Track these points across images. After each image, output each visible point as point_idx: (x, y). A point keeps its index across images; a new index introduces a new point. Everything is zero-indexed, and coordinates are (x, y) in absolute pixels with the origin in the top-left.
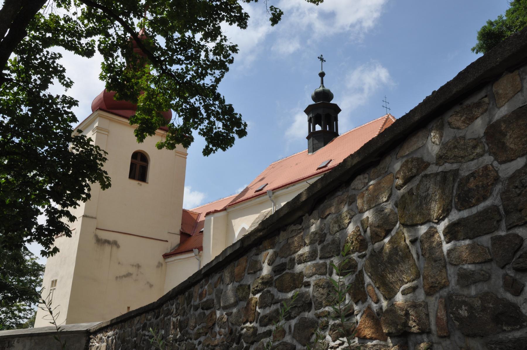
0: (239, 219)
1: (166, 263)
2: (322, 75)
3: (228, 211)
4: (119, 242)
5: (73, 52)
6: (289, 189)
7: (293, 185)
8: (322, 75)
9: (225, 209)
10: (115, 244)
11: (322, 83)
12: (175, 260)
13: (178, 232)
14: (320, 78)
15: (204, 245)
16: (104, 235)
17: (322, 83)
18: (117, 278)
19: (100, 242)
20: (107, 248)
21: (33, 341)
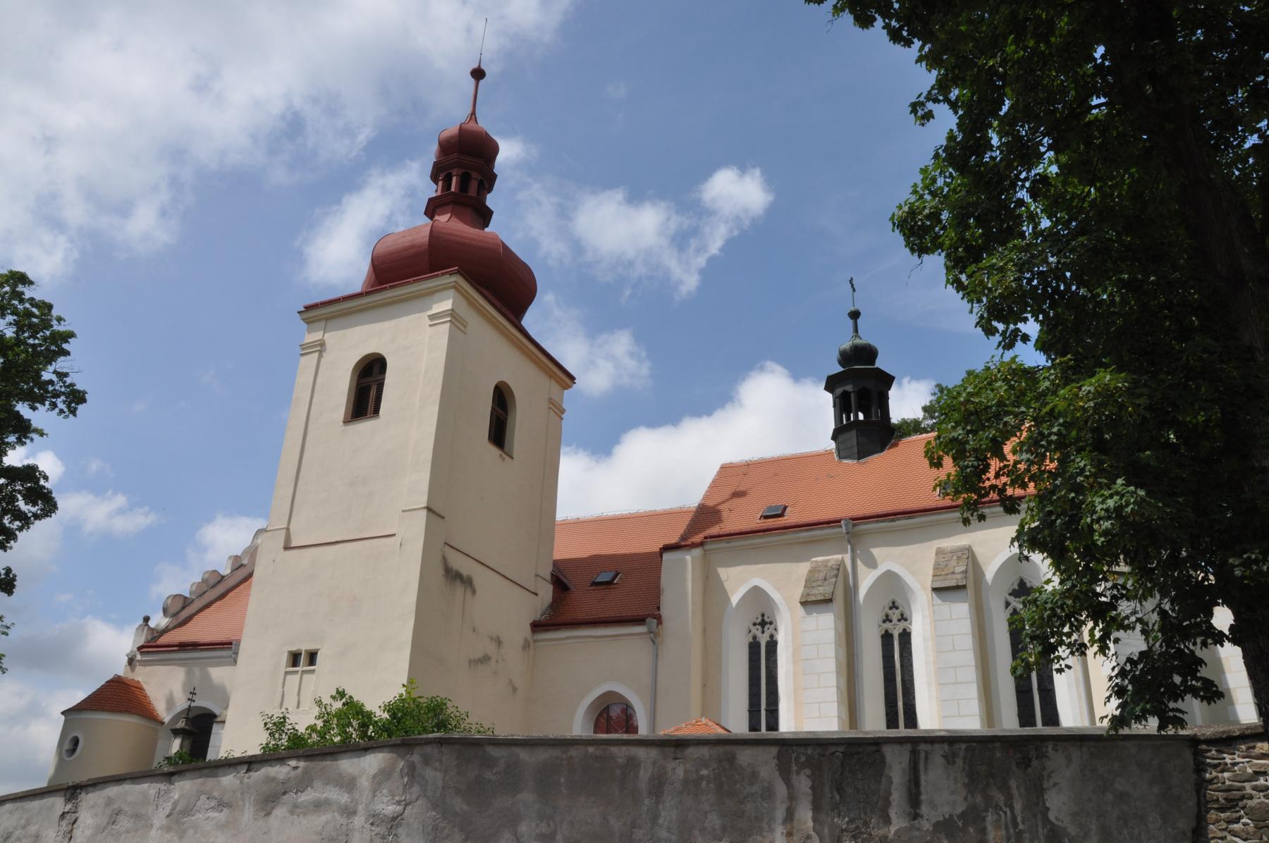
0: (740, 569)
1: (535, 641)
2: (855, 315)
3: (707, 547)
4: (477, 583)
5: (619, 195)
6: (898, 523)
7: (893, 520)
8: (855, 315)
9: (288, 529)
10: (468, 582)
11: (856, 330)
12: (568, 638)
13: (548, 577)
14: (851, 322)
15: (665, 612)
16: (458, 562)
17: (856, 330)
18: (470, 662)
19: (453, 576)
20: (460, 590)
21: (1085, 749)
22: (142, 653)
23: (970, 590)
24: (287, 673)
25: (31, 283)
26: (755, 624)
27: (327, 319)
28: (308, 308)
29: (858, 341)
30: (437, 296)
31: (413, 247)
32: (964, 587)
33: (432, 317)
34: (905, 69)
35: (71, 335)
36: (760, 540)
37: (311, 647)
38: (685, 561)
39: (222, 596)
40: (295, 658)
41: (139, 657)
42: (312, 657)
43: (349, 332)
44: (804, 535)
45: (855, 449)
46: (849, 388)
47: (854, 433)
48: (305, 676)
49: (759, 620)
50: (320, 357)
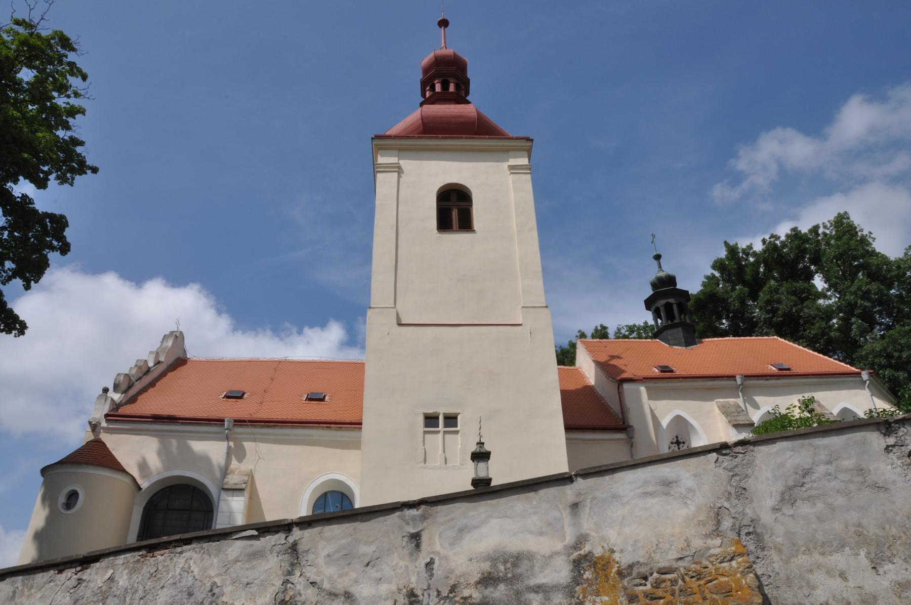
2: (658, 257)
11: (660, 267)
14: (655, 262)
22: (107, 421)
23: (246, 493)
24: (425, 432)
25: (74, 50)
26: (672, 443)
27: (400, 150)
28: (377, 137)
29: (661, 274)
30: (511, 153)
31: (461, 117)
32: (242, 490)
33: (511, 167)
34: (65, 234)
35: (82, 111)
36: (666, 385)
37: (451, 411)
38: (639, 392)
39: (152, 384)
40: (431, 420)
41: (104, 424)
42: (451, 420)
43: (425, 163)
44: (710, 383)
45: (683, 340)
46: (671, 301)
47: (680, 329)
48: (447, 436)
49: (675, 440)
50: (399, 177)
